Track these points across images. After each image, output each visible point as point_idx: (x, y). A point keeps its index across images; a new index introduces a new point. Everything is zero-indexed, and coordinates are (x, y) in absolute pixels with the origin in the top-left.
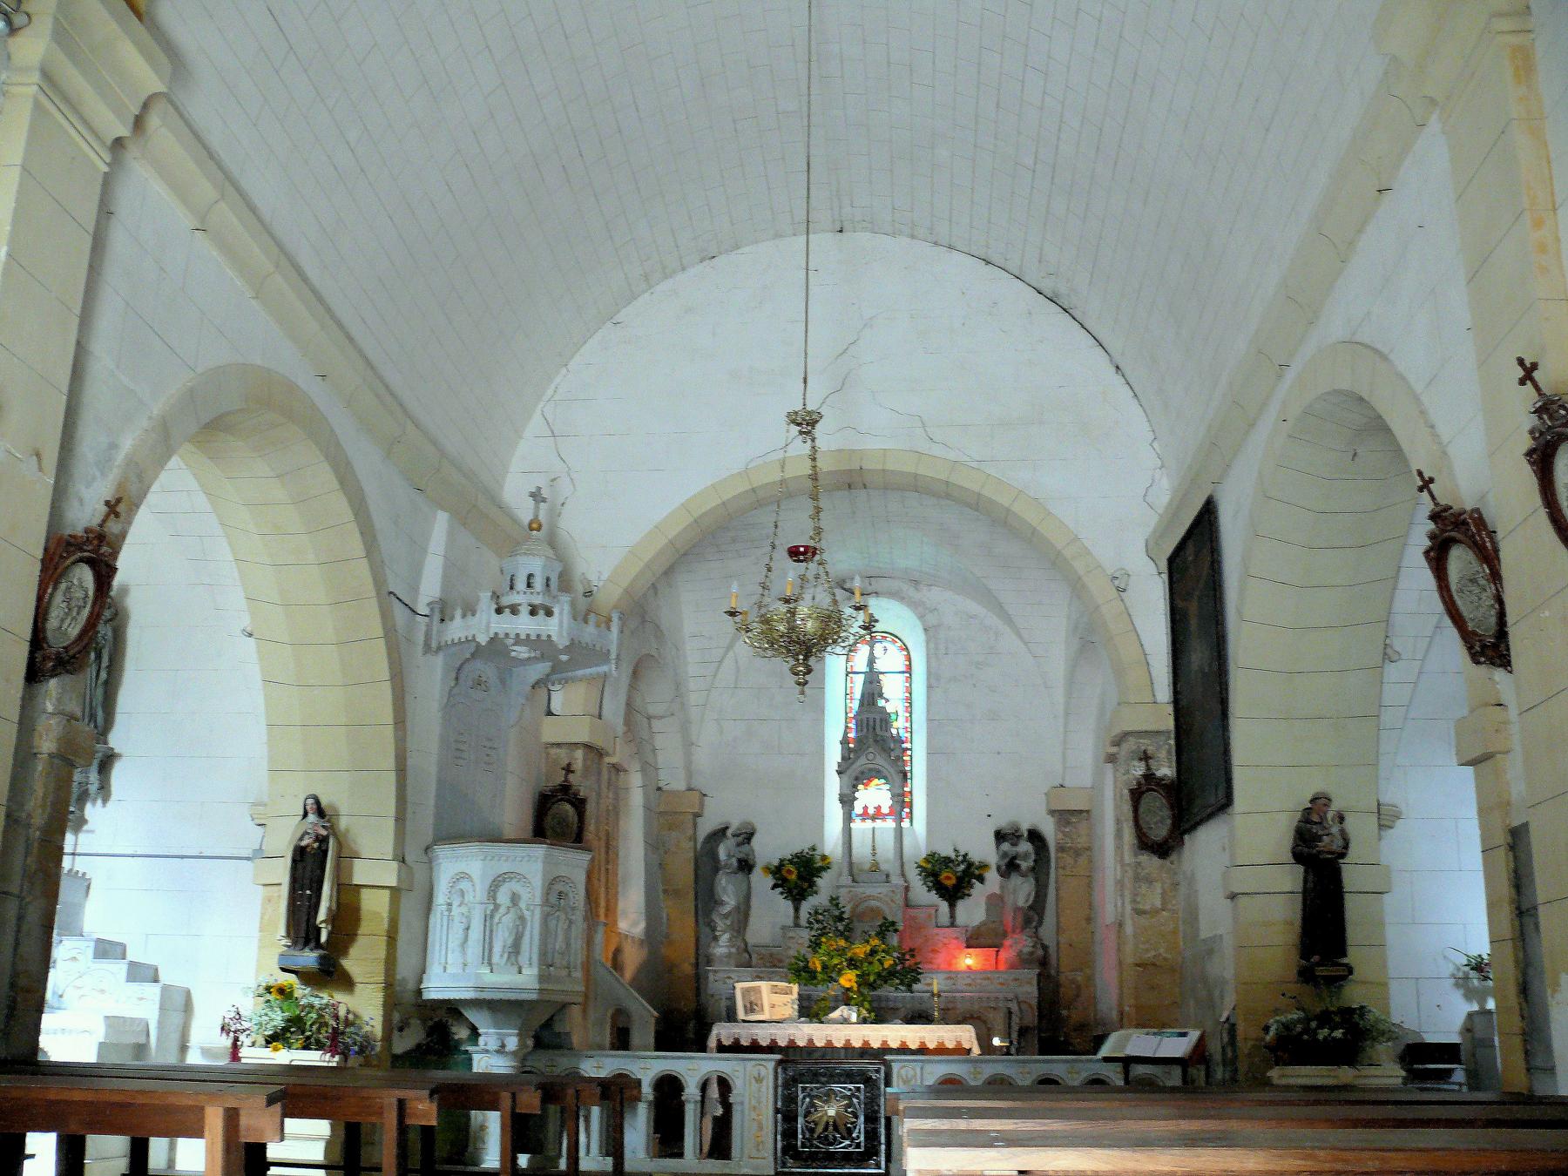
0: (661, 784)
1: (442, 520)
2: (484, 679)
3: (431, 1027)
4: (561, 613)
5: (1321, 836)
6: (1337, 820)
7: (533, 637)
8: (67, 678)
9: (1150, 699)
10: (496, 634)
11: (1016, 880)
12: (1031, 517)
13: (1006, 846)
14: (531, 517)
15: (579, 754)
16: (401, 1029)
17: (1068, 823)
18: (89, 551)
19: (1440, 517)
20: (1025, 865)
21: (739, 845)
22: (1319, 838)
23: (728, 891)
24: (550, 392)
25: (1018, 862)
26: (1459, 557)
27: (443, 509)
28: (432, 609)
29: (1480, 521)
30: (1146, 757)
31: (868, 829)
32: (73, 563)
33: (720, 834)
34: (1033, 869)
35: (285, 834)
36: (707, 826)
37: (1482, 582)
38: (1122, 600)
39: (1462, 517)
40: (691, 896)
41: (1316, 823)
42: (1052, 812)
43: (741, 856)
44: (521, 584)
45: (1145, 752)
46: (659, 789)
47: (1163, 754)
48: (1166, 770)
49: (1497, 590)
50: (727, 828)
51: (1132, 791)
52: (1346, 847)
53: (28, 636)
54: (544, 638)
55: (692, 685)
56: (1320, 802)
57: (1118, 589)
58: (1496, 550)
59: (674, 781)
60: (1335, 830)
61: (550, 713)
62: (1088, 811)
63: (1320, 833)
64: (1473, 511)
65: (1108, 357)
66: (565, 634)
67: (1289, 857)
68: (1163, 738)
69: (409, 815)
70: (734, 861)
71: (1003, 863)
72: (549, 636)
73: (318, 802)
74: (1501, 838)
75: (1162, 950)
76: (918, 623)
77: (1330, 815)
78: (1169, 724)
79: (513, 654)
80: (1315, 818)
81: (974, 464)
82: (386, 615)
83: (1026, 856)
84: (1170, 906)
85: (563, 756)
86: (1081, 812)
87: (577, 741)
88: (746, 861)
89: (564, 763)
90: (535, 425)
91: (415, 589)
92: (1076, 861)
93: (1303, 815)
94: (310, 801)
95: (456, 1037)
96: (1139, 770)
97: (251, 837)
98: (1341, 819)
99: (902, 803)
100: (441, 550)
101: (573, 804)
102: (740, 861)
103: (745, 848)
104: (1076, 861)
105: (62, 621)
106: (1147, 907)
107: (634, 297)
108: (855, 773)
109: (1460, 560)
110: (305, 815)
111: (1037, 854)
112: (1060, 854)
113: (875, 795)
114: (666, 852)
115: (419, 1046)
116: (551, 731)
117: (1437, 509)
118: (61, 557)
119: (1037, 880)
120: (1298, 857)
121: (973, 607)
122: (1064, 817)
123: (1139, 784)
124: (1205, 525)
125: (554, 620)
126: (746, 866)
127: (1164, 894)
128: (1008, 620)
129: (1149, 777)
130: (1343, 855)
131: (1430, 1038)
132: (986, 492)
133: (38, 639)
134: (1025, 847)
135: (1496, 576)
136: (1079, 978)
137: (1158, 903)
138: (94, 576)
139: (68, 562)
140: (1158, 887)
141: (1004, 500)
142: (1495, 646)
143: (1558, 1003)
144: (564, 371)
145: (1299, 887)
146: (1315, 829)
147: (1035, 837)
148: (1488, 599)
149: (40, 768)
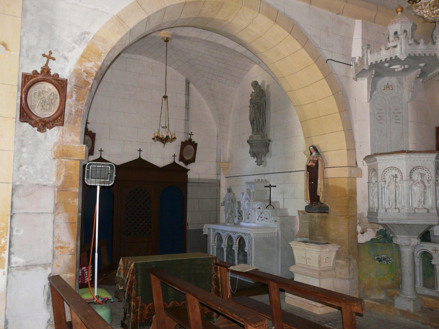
2: (390, 84)
3: (377, 232)
7: (388, 59)
16: (362, 233)
72: (396, 57)
79: (396, 70)
94: (311, 148)
115: (372, 240)
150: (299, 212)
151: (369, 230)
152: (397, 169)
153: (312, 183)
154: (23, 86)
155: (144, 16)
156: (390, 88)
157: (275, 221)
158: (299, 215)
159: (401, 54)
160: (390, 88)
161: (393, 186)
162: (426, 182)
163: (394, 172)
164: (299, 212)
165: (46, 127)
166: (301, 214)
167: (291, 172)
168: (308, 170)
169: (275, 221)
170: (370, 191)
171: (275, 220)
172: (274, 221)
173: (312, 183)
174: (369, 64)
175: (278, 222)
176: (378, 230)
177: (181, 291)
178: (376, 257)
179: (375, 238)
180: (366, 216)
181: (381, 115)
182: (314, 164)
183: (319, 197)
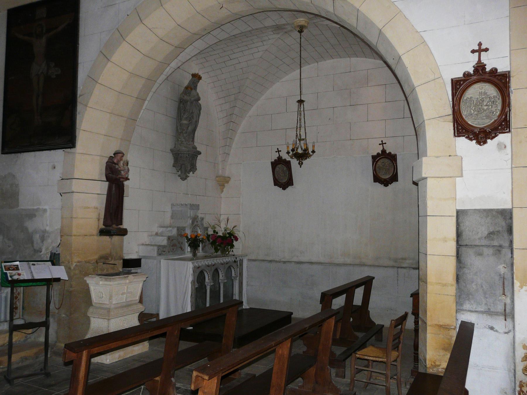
120: (108, 179)
157: (450, 156)
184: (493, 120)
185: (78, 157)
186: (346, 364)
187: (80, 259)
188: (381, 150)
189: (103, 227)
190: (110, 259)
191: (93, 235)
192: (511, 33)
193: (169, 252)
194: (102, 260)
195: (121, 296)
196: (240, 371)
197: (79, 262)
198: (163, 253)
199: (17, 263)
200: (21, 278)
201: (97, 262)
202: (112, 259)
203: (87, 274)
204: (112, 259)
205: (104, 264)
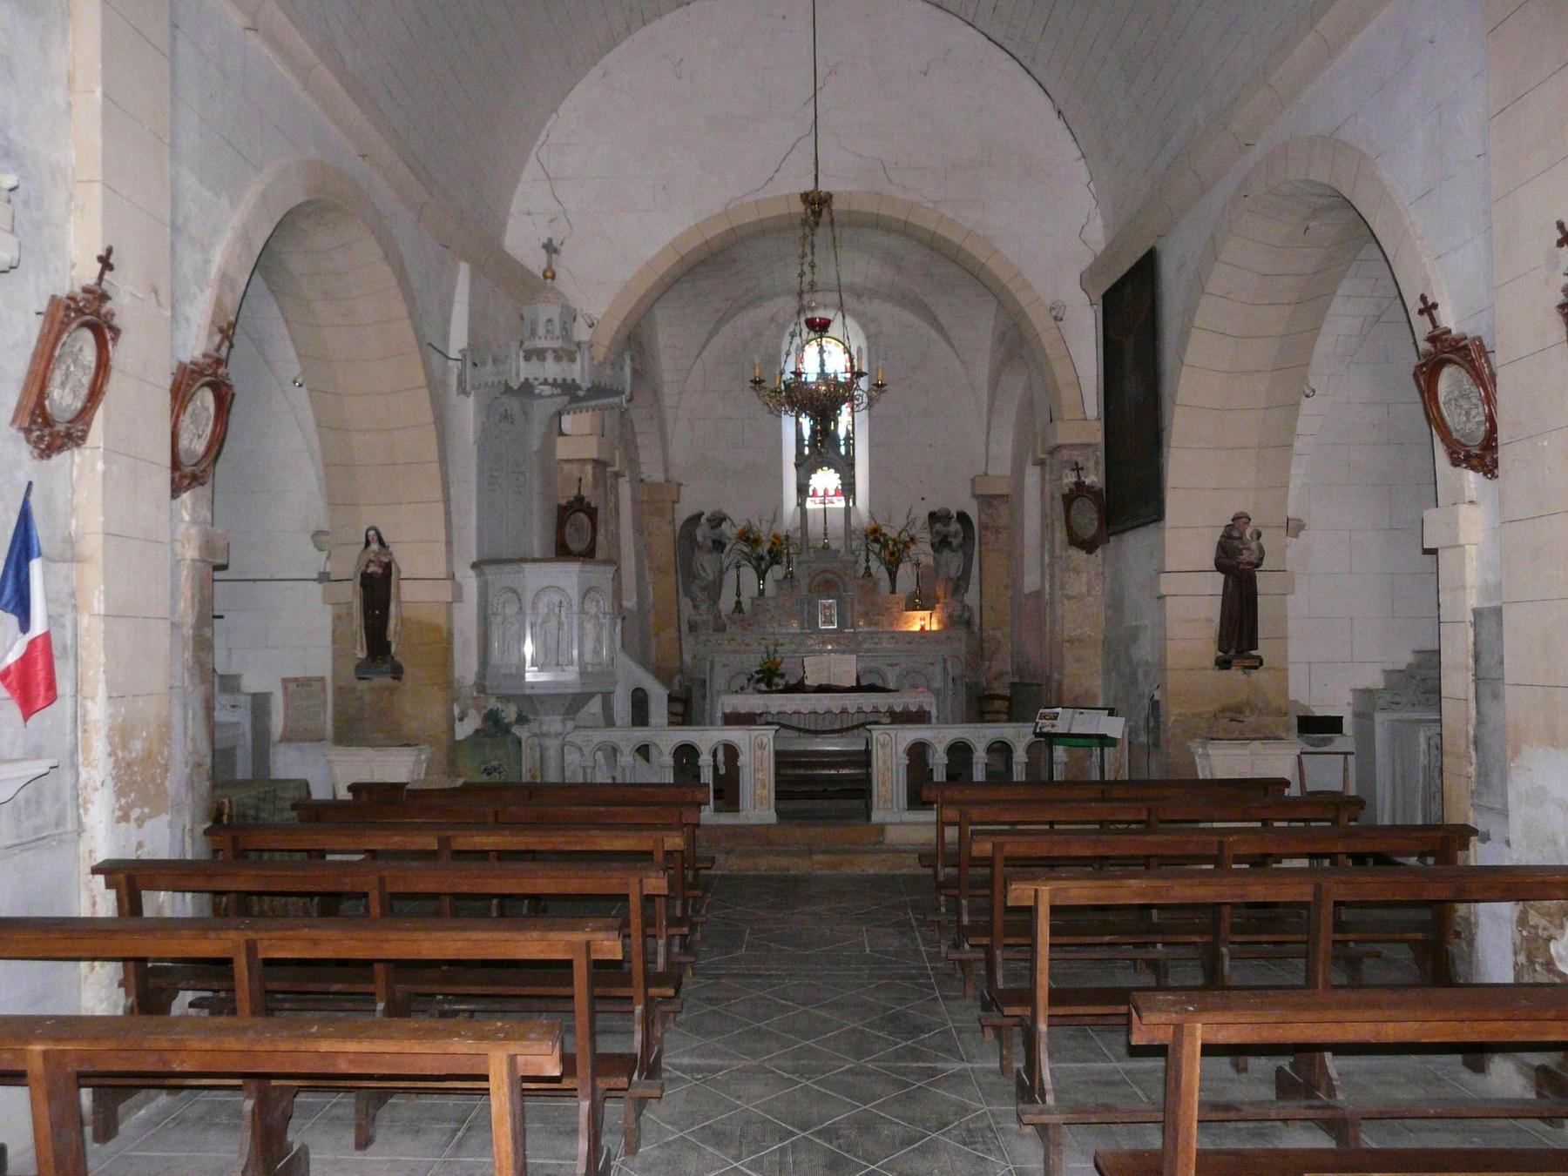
0: (642, 477)
1: (464, 269)
3: (485, 715)
4: (583, 359)
5: (1241, 550)
6: (1255, 536)
7: (559, 381)
8: (199, 490)
9: (1082, 416)
10: (527, 379)
11: (947, 554)
12: (979, 253)
13: (938, 526)
14: (544, 266)
15: (589, 468)
16: (461, 719)
17: (990, 506)
18: (208, 375)
19: (1441, 340)
20: (955, 542)
21: (712, 528)
22: (1240, 552)
23: (706, 563)
24: (542, 137)
25: (950, 539)
26: (1451, 375)
27: (467, 261)
28: (464, 356)
29: (1483, 351)
30: (1077, 468)
31: (819, 510)
32: (198, 389)
33: (695, 519)
34: (961, 546)
35: (348, 563)
36: (684, 512)
37: (1475, 401)
38: (1059, 329)
39: (1463, 343)
40: (672, 570)
41: (1236, 539)
42: (975, 496)
43: (716, 537)
44: (541, 331)
45: (1077, 464)
46: (642, 480)
47: (1091, 464)
48: (1094, 478)
49: (1490, 410)
50: (702, 514)
51: (1064, 497)
52: (1262, 559)
53: (169, 464)
54: (569, 381)
55: (666, 389)
56: (1240, 519)
57: (1056, 318)
58: (1493, 376)
59: (652, 471)
60: (1253, 545)
61: (562, 434)
62: (1007, 496)
63: (1241, 547)
64: (1474, 339)
65: (1049, 101)
66: (586, 376)
67: (1211, 564)
68: (1090, 450)
69: (455, 537)
70: (709, 543)
71: (937, 540)
72: (574, 380)
73: (378, 535)
74: (665, 549)
75: (1087, 629)
76: (861, 332)
77: (1248, 532)
78: (1098, 437)
80: (1236, 534)
81: (931, 205)
82: (426, 364)
83: (956, 534)
84: (1093, 592)
85: (574, 469)
86: (1001, 496)
87: (586, 457)
88: (720, 542)
89: (578, 475)
90: (531, 169)
91: (445, 337)
92: (997, 539)
93: (1225, 531)
94: (372, 533)
95: (506, 721)
96: (1070, 478)
97: (316, 561)
98: (1259, 535)
99: (848, 489)
100: (465, 299)
101: (586, 513)
102: (714, 542)
103: (717, 531)
104: (997, 539)
105: (191, 441)
106: (1075, 594)
107: (616, 44)
108: (806, 467)
109: (1450, 380)
110: (368, 543)
111: (965, 532)
112: (984, 533)
113: (825, 480)
114: (650, 535)
115: (477, 731)
116: (563, 450)
117: (1437, 332)
118: (188, 385)
119: (965, 554)
120: (1220, 567)
121: (910, 318)
122: (987, 501)
123: (1070, 490)
124: (1145, 273)
125: (577, 366)
126: (719, 545)
127: (1089, 583)
128: (941, 330)
129: (1079, 485)
130: (1258, 565)
131: (1319, 713)
132: (940, 231)
133: (176, 463)
134: (955, 526)
135: (1489, 400)
136: (999, 636)
137: (1084, 589)
138: (214, 396)
139: (193, 390)
140: (1084, 578)
141: (956, 238)
142: (1481, 457)
143: (1517, 767)
144: (554, 116)
145: (1220, 590)
146: (1236, 543)
147: (963, 518)
148: (1479, 415)
149: (185, 573)
150: (285, 681)
151: (472, 712)
152: (558, 589)
153: (377, 612)
154: (173, 410)
155: (97, 189)
156: (510, 420)
157: (233, 706)
158: (285, 688)
159: (583, 378)
160: (510, 420)
161: (553, 625)
162: (601, 616)
163: (556, 598)
164: (285, 681)
165: (939, 622)
166: (292, 686)
167: (255, 580)
168: (363, 585)
169: (233, 706)
170: (99, 602)
171: (233, 703)
172: (228, 707)
173: (377, 612)
174: (522, 380)
175: (243, 710)
176: (486, 711)
177: (984, 827)
178: (483, 767)
179: (480, 727)
180: (472, 682)
181: (496, 474)
182: (380, 571)
183: (388, 645)
184: (459, 782)
185: (1169, 535)
186: (406, 325)
187: (1183, 711)
188: (63, 291)
189: (1220, 654)
190: (1247, 712)
191: (1206, 669)
192: (290, 712)
193: (1413, 705)
194: (1228, 714)
195: (1470, 801)
196: (102, 587)
197: (1180, 714)
198: (1394, 706)
199: (1059, 710)
200: (1053, 731)
201: (1215, 715)
202: (1252, 712)
203: (1194, 736)
204: (1252, 712)
205: (1231, 720)
